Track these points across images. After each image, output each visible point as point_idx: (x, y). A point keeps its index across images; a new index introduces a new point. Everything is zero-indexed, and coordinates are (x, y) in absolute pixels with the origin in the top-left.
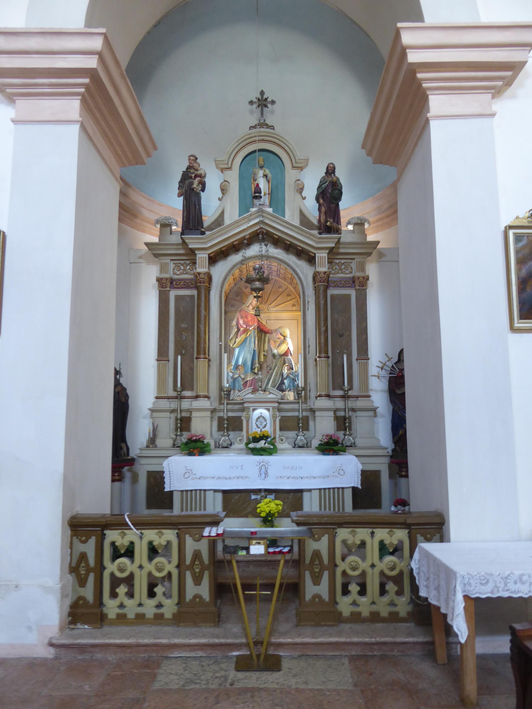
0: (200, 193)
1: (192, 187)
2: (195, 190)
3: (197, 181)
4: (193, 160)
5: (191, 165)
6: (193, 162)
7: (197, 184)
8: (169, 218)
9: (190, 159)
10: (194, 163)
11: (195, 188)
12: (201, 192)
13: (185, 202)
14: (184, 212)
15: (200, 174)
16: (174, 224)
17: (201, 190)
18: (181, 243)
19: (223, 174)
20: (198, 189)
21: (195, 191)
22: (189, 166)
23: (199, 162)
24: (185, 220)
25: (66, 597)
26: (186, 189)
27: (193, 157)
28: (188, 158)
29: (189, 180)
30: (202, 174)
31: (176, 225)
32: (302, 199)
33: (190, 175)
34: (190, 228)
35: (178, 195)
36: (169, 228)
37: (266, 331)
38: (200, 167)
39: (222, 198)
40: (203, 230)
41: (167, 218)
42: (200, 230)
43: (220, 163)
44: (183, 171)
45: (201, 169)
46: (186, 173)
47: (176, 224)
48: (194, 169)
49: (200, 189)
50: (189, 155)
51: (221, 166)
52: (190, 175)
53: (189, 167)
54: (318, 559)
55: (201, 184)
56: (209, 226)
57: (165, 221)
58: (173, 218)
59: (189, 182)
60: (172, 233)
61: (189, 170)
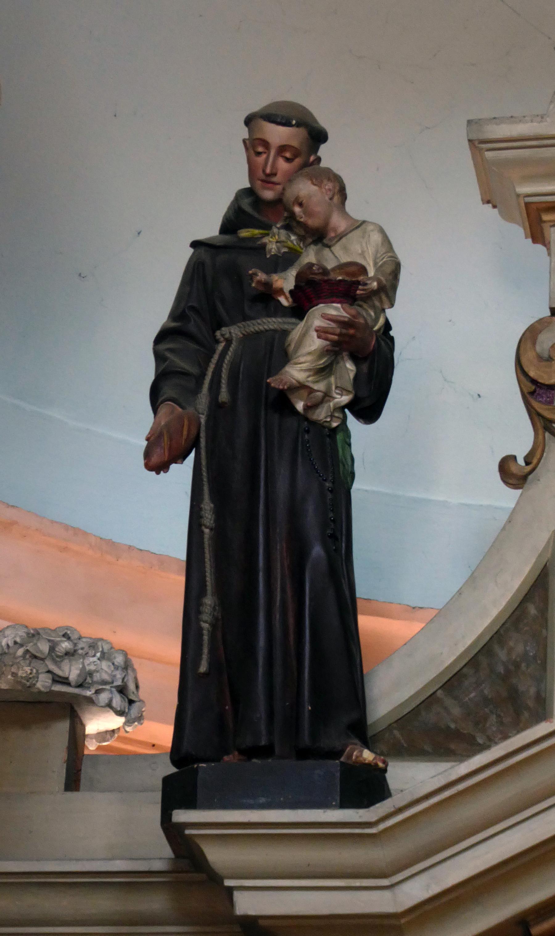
0: (344, 426)
1: (274, 382)
2: (300, 406)
3: (321, 333)
4: (282, 149)
5: (268, 195)
6: (282, 165)
7: (324, 352)
8: (66, 645)
9: (266, 144)
10: (290, 179)
11: (301, 386)
12: (352, 422)
13: (207, 506)
14: (202, 593)
15: (342, 267)
16: (104, 697)
17: (350, 406)
18: (158, 866)
19: (540, 247)
20: (327, 396)
21: (303, 418)
22: (249, 192)
23: (337, 169)
24: (203, 668)
25: (67, 548)
26: (224, 396)
27: (287, 123)
28: (244, 133)
29: (246, 318)
30: (363, 270)
31: (117, 701)
32: (471, 118)
33: (261, 276)
34: (248, 741)
35: (147, 454)
36: (64, 726)
37: (286, 159)
38: (349, 206)
39: (528, 461)
40: (368, 755)
41: (44, 647)
42: (335, 754)
43: (523, 163)
44: (195, 244)
45: (360, 225)
46: (223, 257)
47: (122, 690)
48: (288, 227)
49: (345, 399)
50: (256, 106)
51: (525, 189)
52: (261, 276)
53: (246, 204)
54: (426, 625)
55: (355, 359)
56: (415, 712)
57: (25, 670)
58: (93, 645)
59: (247, 338)
60: (86, 771)
61: (244, 233)
